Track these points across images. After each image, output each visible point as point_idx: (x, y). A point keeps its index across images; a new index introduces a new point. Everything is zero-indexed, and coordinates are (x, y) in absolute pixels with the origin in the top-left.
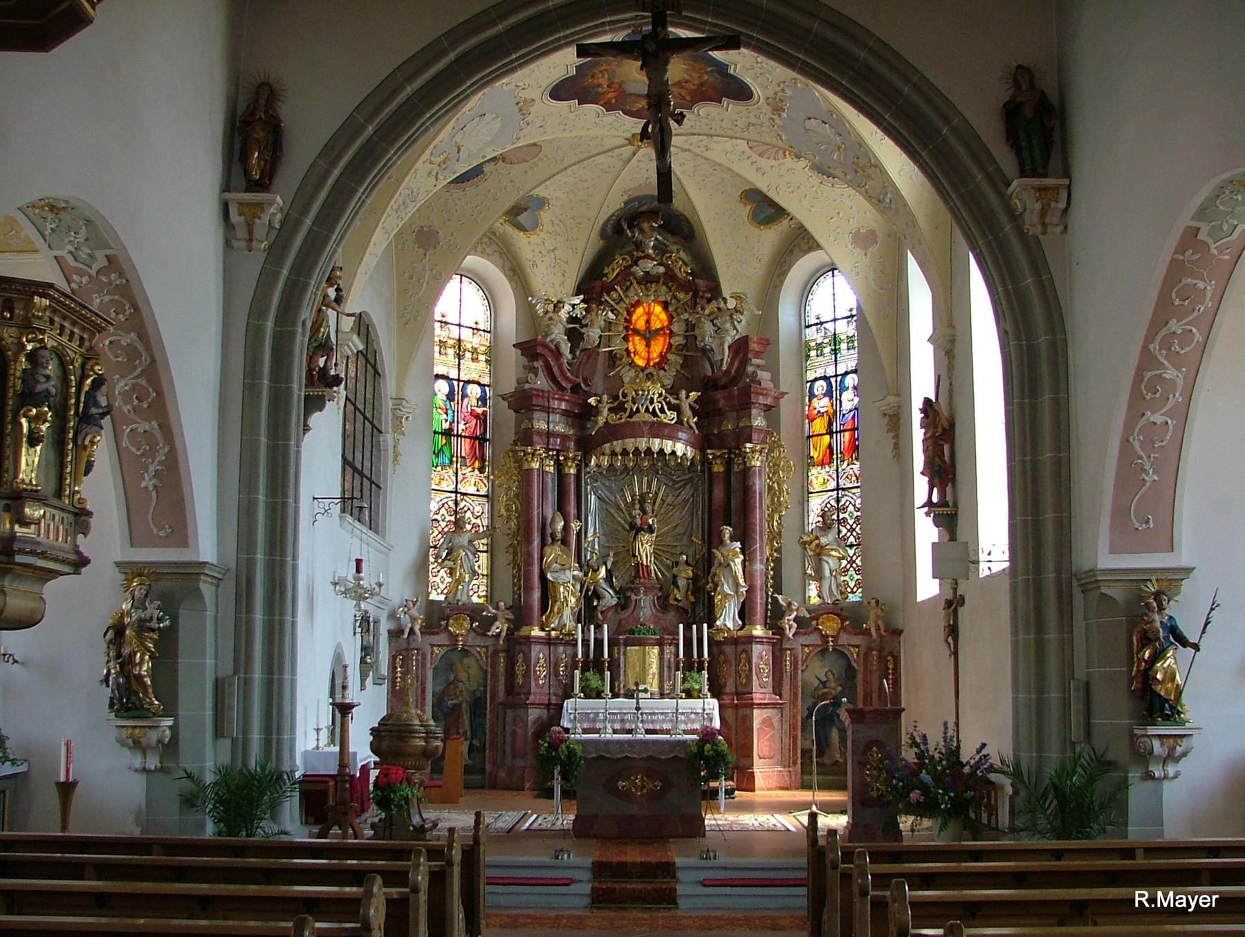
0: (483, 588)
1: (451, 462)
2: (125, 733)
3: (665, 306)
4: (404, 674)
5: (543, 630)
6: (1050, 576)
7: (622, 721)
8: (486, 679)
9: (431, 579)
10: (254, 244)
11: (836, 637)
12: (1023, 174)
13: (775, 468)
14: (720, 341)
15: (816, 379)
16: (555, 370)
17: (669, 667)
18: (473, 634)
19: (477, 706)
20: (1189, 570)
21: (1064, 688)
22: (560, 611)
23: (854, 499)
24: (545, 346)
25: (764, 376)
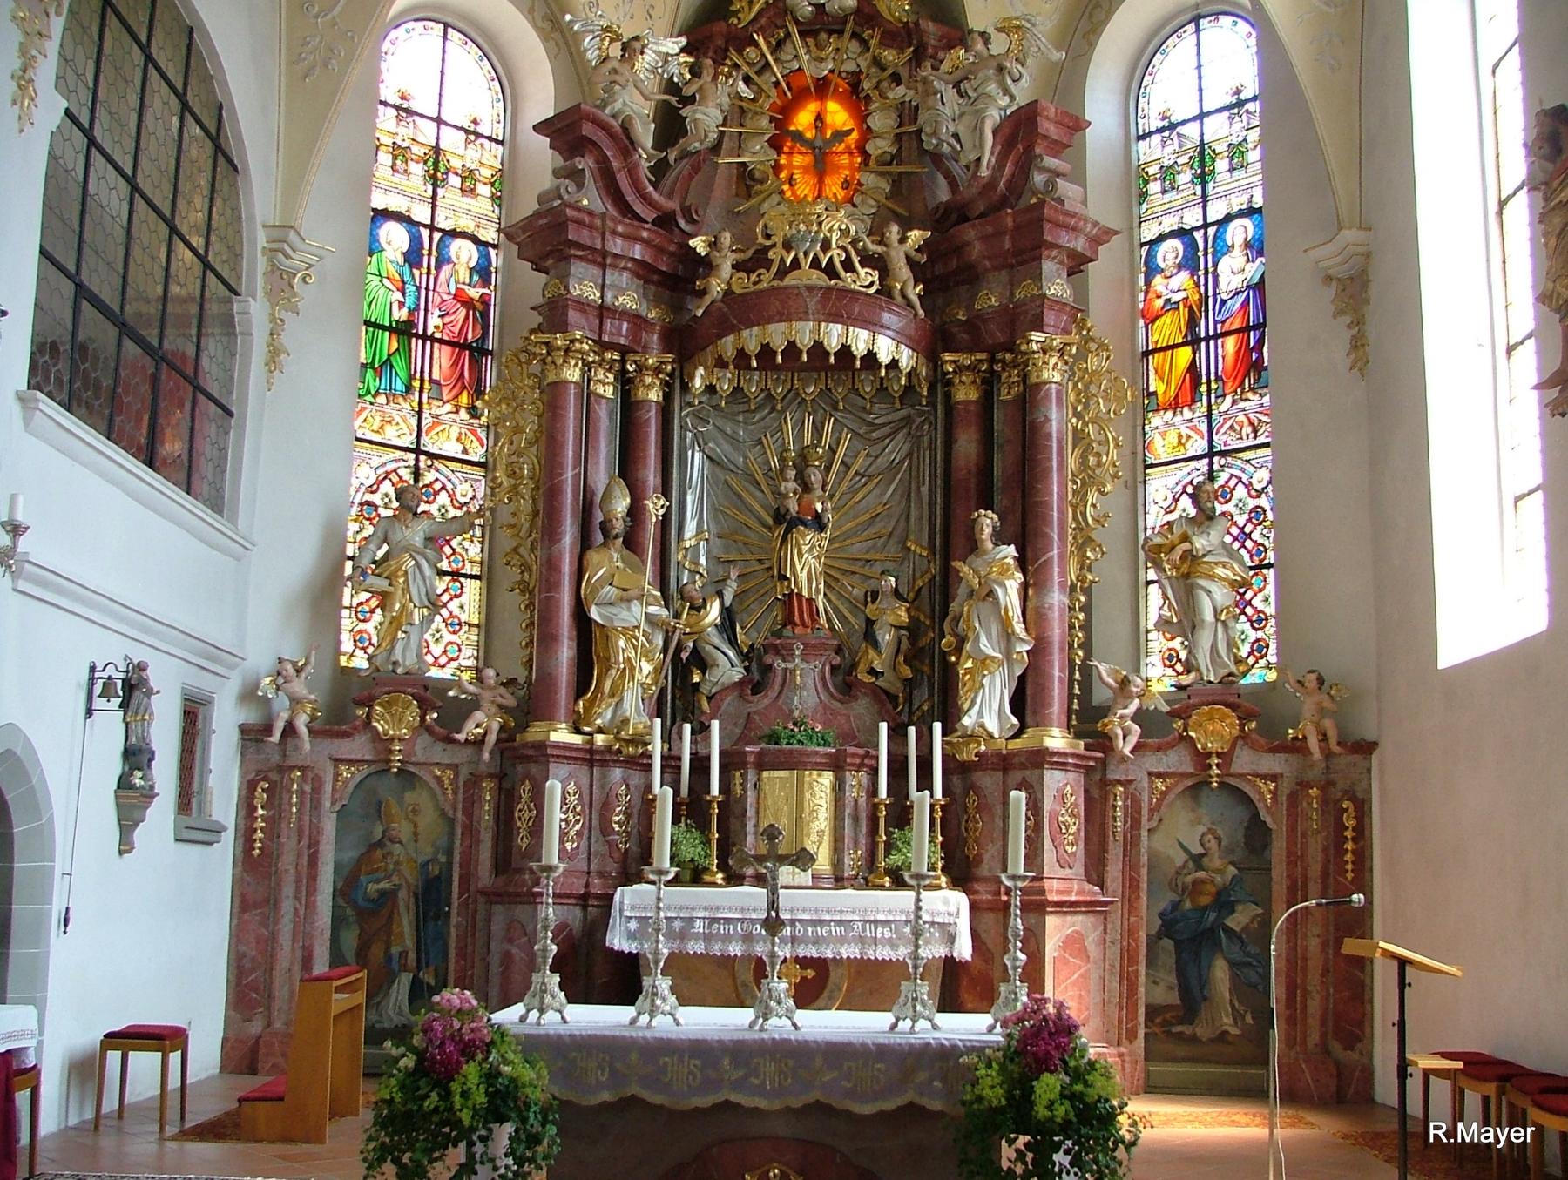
0: (468, 652)
1: (409, 389)
4: (273, 823)
5: (577, 731)
8: (452, 834)
14: (968, 126)
15: (1161, 238)
16: (623, 180)
17: (856, 819)
18: (425, 739)
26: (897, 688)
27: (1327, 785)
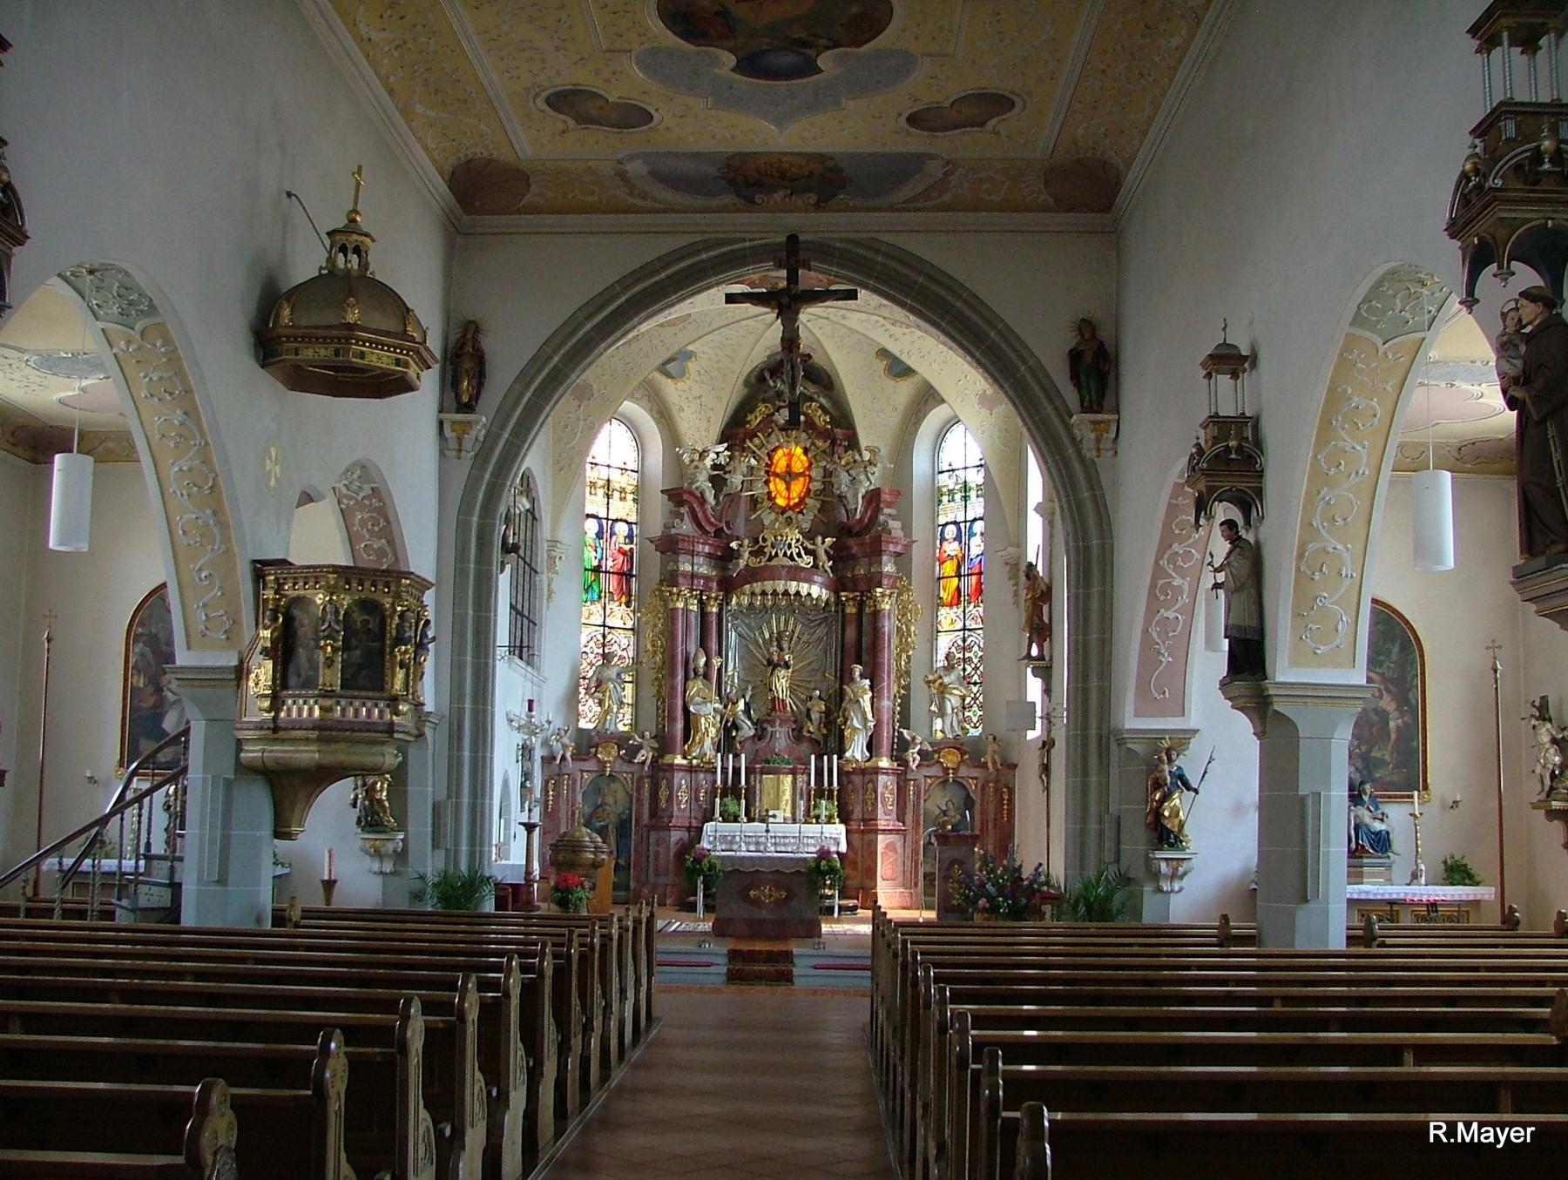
0: (628, 716)
3: (806, 451)
4: (557, 797)
6: (1093, 732)
7: (757, 843)
10: (463, 454)
12: (1084, 410)
16: (700, 515)
19: (623, 827)
21: (1101, 822)
22: (702, 741)
23: (976, 639)
24: (691, 493)
25: (895, 525)
26: (820, 738)
27: (997, 782)
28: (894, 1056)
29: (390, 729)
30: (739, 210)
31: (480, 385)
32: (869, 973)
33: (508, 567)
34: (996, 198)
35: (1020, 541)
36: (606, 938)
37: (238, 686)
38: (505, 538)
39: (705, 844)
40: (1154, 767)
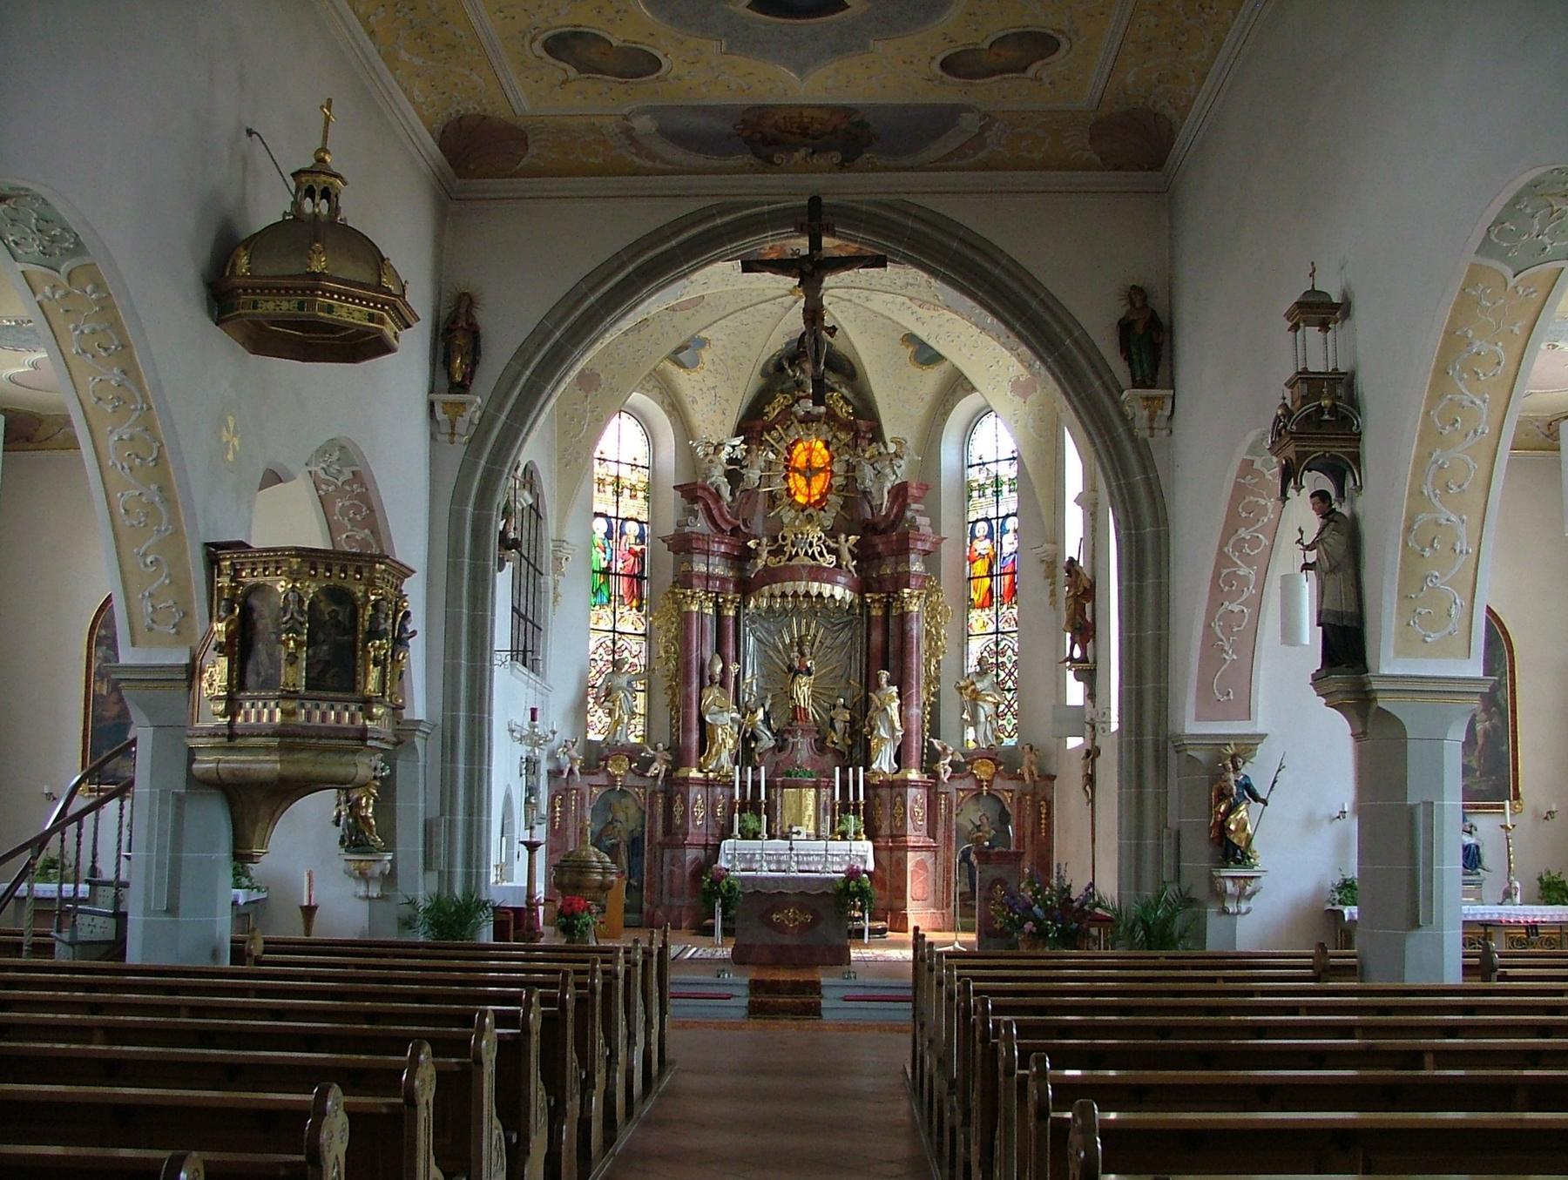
0: (640, 727)
2: (352, 866)
3: (827, 445)
4: (564, 814)
6: (1149, 738)
7: (779, 862)
9: (589, 719)
11: (990, 782)
13: (933, 613)
14: (880, 486)
16: (715, 512)
19: (635, 844)
20: (1263, 736)
21: (1159, 837)
22: (718, 753)
23: (1011, 643)
24: (705, 489)
25: (923, 521)
27: (1034, 795)
28: (952, 1117)
29: (363, 735)
30: (757, 172)
31: (474, 363)
32: (910, 1005)
33: (509, 566)
34: (1037, 156)
35: (1058, 538)
36: (610, 975)
37: (190, 687)
38: (503, 534)
39: (722, 863)
40: (1217, 776)
